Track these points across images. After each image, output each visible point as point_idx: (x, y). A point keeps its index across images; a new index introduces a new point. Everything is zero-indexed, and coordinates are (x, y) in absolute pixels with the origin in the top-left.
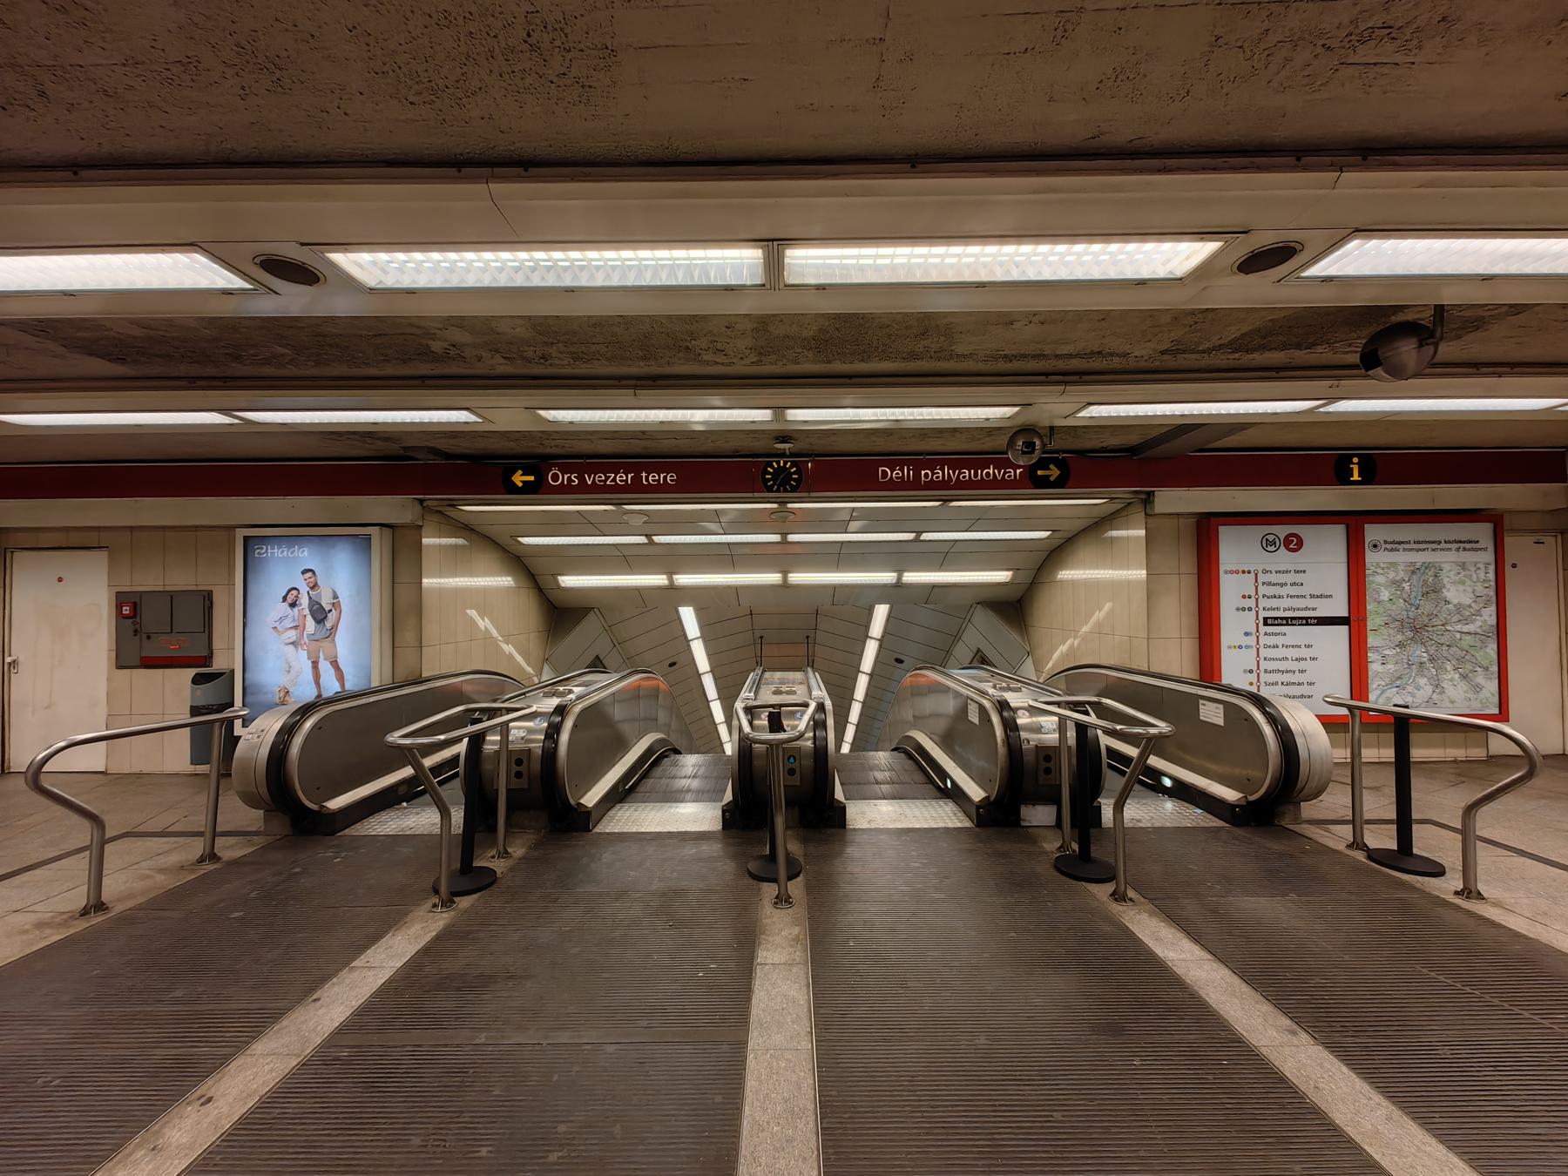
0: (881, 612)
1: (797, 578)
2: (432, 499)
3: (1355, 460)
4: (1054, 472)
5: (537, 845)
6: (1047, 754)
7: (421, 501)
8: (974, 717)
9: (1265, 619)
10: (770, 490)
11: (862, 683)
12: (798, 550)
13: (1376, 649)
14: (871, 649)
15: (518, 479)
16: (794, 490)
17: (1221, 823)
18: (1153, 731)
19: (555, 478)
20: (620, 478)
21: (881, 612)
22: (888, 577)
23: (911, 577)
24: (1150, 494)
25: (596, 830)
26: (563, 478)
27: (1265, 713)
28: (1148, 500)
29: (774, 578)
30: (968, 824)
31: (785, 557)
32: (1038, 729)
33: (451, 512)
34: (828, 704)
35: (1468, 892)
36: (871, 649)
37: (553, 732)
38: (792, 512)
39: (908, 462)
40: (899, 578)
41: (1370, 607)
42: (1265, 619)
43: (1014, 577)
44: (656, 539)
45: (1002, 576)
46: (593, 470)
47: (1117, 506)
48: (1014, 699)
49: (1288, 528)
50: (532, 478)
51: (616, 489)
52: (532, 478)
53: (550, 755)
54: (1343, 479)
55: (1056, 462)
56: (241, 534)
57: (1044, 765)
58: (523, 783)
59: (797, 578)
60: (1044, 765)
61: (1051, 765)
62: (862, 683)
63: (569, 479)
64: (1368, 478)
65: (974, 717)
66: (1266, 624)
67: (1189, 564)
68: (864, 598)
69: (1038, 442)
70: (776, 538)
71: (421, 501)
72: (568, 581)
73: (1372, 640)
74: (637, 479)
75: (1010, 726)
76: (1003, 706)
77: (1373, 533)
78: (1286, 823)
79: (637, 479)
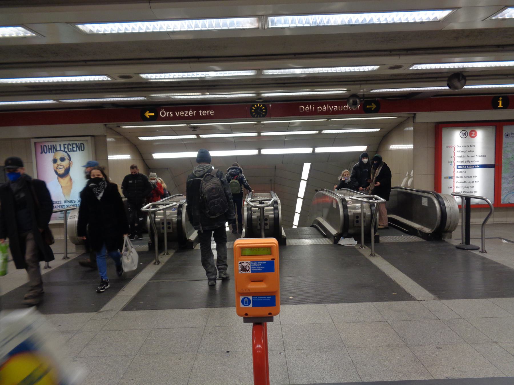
0: (307, 167)
1: (264, 152)
2: (111, 125)
3: (501, 99)
4: (374, 106)
5: (176, 252)
6: (357, 216)
7: (106, 125)
8: (335, 206)
9: (458, 166)
10: (254, 116)
11: (299, 203)
12: (264, 139)
13: (505, 178)
14: (303, 185)
15: (148, 114)
16: (264, 116)
17: (424, 240)
18: (379, 201)
19: (163, 114)
20: (191, 113)
21: (307, 167)
22: (308, 150)
23: (319, 150)
24: (415, 114)
25: (195, 249)
26: (166, 114)
27: (440, 203)
28: (414, 117)
29: (255, 152)
30: (331, 243)
31: (259, 143)
32: (355, 208)
33: (118, 129)
34: (279, 201)
35: (484, 251)
36: (303, 185)
37: (179, 213)
38: (263, 124)
39: (312, 104)
40: (314, 150)
41: (503, 161)
42: (458, 166)
43: (367, 149)
44: (201, 136)
45: (363, 148)
46: (179, 110)
47: (401, 119)
48: (347, 198)
49: (469, 126)
50: (153, 114)
51: (189, 118)
52: (153, 114)
53: (179, 222)
54: (495, 106)
55: (375, 102)
56: (33, 141)
57: (356, 219)
58: (171, 231)
59: (264, 152)
60: (356, 219)
61: (359, 219)
62: (299, 203)
63: (169, 114)
64: (506, 106)
65: (335, 206)
66: (458, 168)
67: (431, 144)
68: (306, 158)
69: (358, 100)
70: (255, 134)
71: (106, 125)
72: (157, 156)
73: (504, 175)
74: (197, 113)
75: (345, 207)
76: (343, 200)
77: (506, 129)
78: (446, 240)
79: (197, 113)
